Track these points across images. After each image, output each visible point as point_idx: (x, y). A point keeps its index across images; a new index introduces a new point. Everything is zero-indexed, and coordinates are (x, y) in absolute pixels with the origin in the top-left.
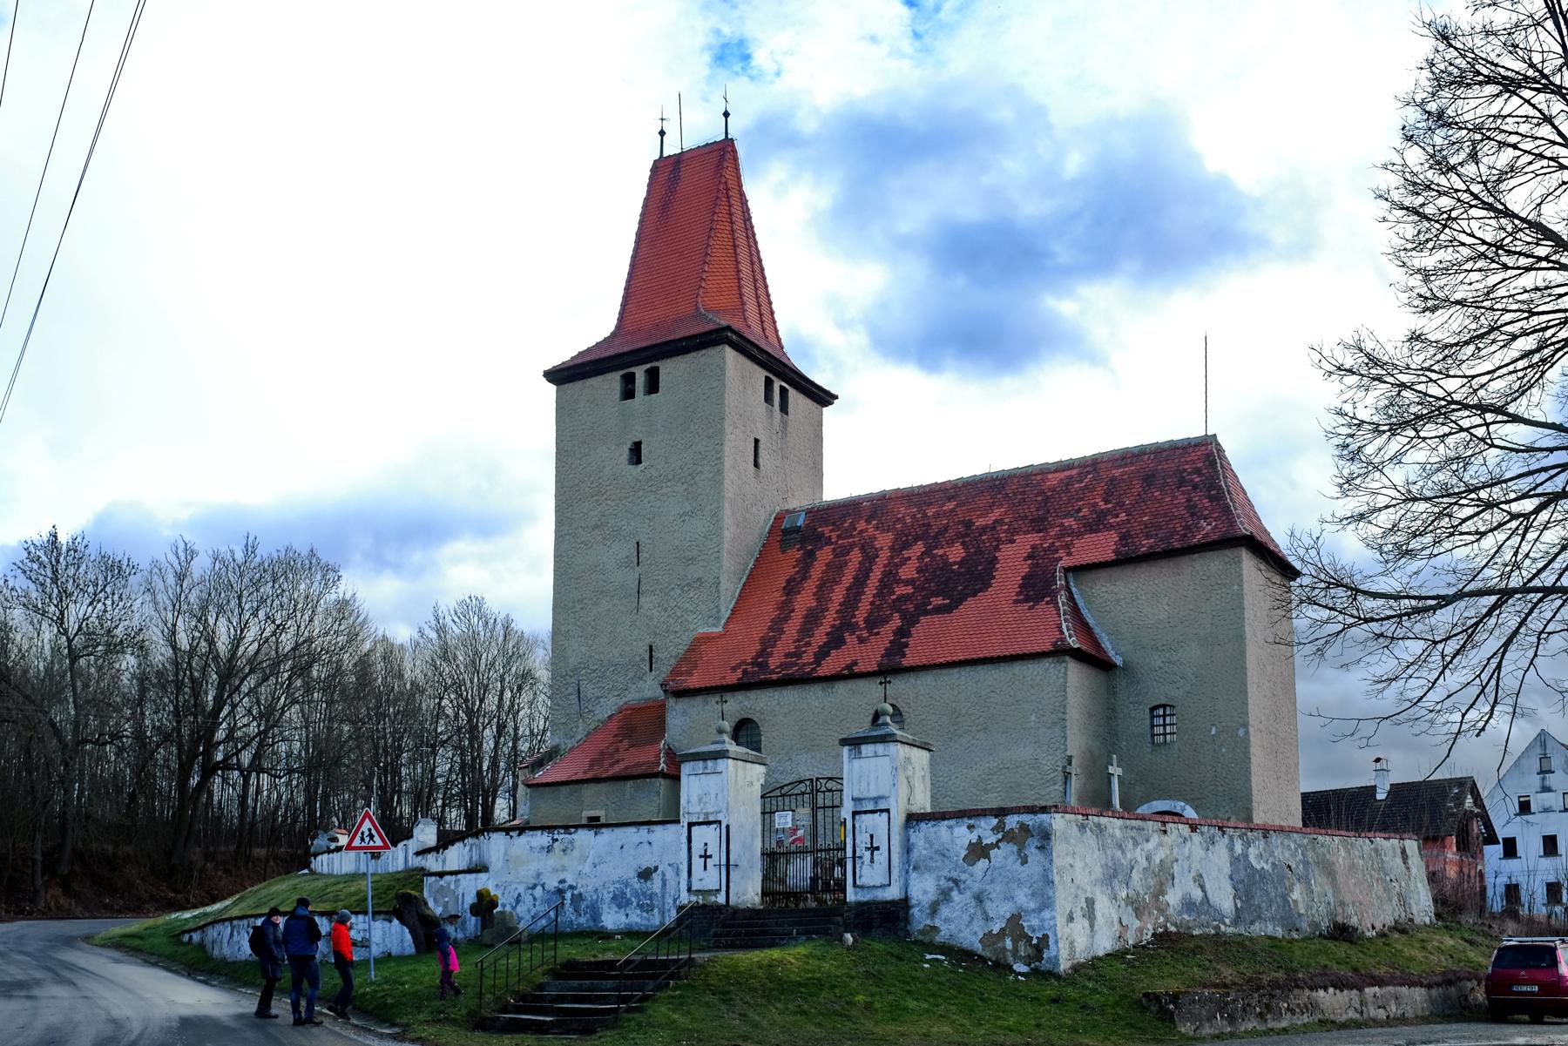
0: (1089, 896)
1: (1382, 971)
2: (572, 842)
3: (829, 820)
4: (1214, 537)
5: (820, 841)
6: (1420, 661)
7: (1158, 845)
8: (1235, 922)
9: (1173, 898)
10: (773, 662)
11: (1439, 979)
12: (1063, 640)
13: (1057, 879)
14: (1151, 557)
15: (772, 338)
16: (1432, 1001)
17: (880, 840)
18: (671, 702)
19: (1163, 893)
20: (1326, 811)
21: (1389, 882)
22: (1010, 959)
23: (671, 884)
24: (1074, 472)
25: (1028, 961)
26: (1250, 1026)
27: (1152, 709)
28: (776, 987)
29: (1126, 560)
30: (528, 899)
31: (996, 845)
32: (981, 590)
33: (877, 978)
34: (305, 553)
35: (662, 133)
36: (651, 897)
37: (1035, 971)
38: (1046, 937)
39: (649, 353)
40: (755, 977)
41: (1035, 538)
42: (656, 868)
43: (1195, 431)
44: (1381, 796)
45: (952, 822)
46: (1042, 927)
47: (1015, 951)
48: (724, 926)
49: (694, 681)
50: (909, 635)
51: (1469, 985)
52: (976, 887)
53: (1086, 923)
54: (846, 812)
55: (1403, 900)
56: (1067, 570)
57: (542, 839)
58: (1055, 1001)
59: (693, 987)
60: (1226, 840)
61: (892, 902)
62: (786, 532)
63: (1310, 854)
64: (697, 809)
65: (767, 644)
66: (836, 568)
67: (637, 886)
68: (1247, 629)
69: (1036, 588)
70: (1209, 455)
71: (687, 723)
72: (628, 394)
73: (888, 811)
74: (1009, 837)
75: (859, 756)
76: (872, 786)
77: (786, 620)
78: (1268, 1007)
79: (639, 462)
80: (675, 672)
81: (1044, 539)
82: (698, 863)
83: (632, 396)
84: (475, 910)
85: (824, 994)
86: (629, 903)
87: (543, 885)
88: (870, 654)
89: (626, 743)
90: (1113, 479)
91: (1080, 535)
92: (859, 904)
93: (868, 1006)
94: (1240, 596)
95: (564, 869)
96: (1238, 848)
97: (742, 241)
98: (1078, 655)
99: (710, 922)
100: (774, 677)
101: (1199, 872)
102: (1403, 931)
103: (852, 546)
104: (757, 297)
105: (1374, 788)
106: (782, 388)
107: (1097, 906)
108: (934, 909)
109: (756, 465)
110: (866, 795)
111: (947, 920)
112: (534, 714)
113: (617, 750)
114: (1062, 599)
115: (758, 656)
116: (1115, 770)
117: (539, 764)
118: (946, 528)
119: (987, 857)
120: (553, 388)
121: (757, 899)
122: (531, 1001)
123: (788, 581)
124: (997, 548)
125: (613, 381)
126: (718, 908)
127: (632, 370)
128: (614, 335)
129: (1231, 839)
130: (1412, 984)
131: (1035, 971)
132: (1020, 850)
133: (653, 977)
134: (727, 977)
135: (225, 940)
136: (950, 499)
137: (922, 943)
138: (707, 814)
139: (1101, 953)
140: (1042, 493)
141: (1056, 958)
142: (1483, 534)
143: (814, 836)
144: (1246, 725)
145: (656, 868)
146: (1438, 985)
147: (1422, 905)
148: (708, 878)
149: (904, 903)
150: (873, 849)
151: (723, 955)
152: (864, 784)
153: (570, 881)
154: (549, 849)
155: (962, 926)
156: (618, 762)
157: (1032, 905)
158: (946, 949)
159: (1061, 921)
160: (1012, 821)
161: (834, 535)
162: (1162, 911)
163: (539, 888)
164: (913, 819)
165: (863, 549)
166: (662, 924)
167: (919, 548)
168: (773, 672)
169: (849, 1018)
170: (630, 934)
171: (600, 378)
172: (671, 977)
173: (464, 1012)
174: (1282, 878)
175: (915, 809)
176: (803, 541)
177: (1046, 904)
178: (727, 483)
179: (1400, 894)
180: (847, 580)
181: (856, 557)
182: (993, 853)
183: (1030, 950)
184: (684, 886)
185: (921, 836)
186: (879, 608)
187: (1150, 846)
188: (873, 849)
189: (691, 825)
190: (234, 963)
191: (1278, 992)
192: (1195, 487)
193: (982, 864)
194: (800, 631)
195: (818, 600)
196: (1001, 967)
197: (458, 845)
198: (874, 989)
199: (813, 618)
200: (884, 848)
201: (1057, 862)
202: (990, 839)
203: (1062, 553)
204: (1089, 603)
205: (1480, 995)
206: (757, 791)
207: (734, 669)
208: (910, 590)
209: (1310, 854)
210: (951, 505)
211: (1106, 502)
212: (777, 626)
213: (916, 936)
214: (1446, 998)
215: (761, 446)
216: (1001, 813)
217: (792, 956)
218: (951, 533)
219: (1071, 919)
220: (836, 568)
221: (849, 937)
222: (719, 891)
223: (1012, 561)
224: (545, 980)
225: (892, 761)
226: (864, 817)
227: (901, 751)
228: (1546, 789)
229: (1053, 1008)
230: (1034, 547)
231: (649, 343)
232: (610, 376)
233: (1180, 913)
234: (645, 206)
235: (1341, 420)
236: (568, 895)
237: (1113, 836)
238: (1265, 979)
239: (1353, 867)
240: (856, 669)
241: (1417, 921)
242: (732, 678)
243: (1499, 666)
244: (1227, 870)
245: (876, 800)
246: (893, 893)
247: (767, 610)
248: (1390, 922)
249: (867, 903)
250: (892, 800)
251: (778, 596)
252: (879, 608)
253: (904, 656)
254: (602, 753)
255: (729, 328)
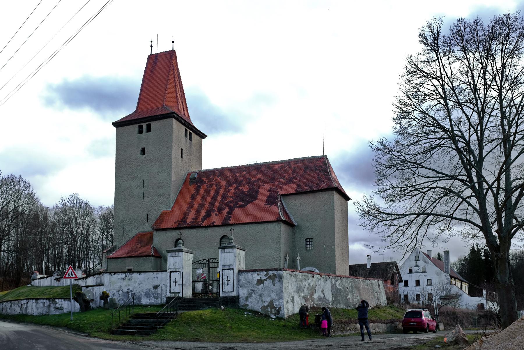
0: (293, 294)
1: (374, 319)
2: (132, 277)
3: (213, 272)
4: (326, 187)
5: (211, 278)
6: (395, 232)
7: (311, 281)
8: (333, 304)
9: (315, 297)
10: (188, 221)
11: (389, 321)
12: (280, 217)
13: (284, 290)
14: (307, 192)
15: (187, 116)
16: (387, 328)
17: (231, 278)
18: (155, 232)
19: (313, 295)
20: (357, 271)
21: (375, 293)
22: (270, 314)
23: (164, 292)
24: (283, 165)
25: (275, 315)
26: (339, 334)
27: (306, 239)
28: (203, 322)
29: (299, 193)
30: (117, 295)
31: (266, 280)
32: (254, 200)
33: (232, 319)
34: (18, 176)
35: (151, 46)
36: (158, 294)
37: (277, 318)
38: (280, 307)
39: (147, 119)
40: (196, 318)
41: (271, 185)
42: (159, 285)
43: (320, 154)
44: (368, 267)
45: (252, 273)
46: (279, 305)
47: (271, 312)
48: (181, 304)
49: (162, 226)
50: (231, 214)
51: (397, 323)
52: (260, 292)
53: (292, 304)
54: (219, 269)
55: (378, 298)
56: (281, 195)
57: (122, 276)
58: (284, 326)
59: (178, 321)
60: (330, 280)
61: (234, 297)
62: (191, 179)
63: (353, 284)
64: (173, 267)
65: (186, 215)
66: (208, 191)
67: (153, 291)
68: (335, 216)
69: (271, 201)
70: (325, 162)
71: (162, 241)
72: (140, 132)
73: (233, 269)
74: (269, 277)
75: (224, 252)
76: (228, 261)
77: (192, 207)
78: (344, 328)
79: (144, 154)
80: (156, 223)
81: (273, 185)
82: (173, 284)
83: (142, 133)
84: (101, 298)
85: (217, 323)
86: (150, 296)
87: (122, 290)
88: (220, 219)
89: (139, 245)
90: (295, 168)
91: (285, 185)
92: (224, 297)
93: (231, 327)
94: (333, 206)
95: (129, 285)
96: (334, 282)
97: (178, 84)
98: (284, 222)
99: (178, 303)
100: (189, 226)
101: (322, 290)
102: (379, 308)
103: (213, 184)
104: (183, 103)
105: (366, 265)
106: (190, 132)
107: (295, 299)
108: (247, 299)
109: (182, 157)
110: (226, 264)
111: (251, 302)
112: (96, 234)
113: (137, 247)
114: (279, 204)
115: (183, 219)
116: (299, 258)
117: (110, 251)
118: (243, 180)
119: (263, 283)
120: (115, 128)
121: (191, 295)
122: (127, 325)
123: (192, 195)
124: (259, 188)
125: (135, 127)
126: (179, 298)
127: (142, 124)
128: (135, 112)
129: (332, 279)
130: (382, 323)
131: (277, 318)
132: (273, 282)
133: (166, 318)
134: (188, 318)
135: (8, 308)
136: (244, 171)
137: (243, 309)
138: (176, 269)
139: (296, 313)
140: (273, 171)
141: (284, 314)
142: (413, 196)
143: (209, 276)
144: (334, 245)
145: (159, 285)
146: (389, 323)
147: (383, 300)
148: (176, 289)
149: (238, 297)
150: (228, 281)
151: (186, 312)
152: (226, 261)
153: (131, 289)
154: (124, 279)
155: (255, 304)
156: (137, 251)
157: (276, 298)
158: (250, 311)
159: (285, 303)
160: (271, 273)
161: (207, 181)
162: (312, 301)
163: (121, 291)
164: (240, 272)
165: (216, 186)
166: (161, 302)
167: (234, 186)
168: (188, 224)
169: (226, 330)
170: (152, 306)
171: (131, 126)
172: (171, 318)
173: (107, 329)
174: (346, 291)
175: (241, 269)
176: (197, 182)
177: (281, 298)
178: (173, 162)
179: (377, 297)
180: (211, 195)
181: (214, 188)
182: (265, 282)
183: (276, 312)
184: (168, 291)
185: (243, 277)
186: (222, 205)
187: (309, 281)
188: (228, 281)
189: (171, 272)
190: (13, 315)
191: (346, 324)
192: (320, 171)
193: (261, 285)
194: (196, 211)
195: (202, 201)
196: (267, 316)
197: (91, 277)
198: (231, 322)
199: (200, 207)
200: (232, 280)
201: (284, 285)
202: (264, 278)
203: (279, 190)
204: (287, 206)
205: (400, 326)
206: (191, 262)
207: (175, 223)
208: (231, 199)
209: (353, 284)
210: (244, 173)
211: (293, 175)
212: (189, 209)
213: (241, 307)
214: (391, 327)
215: (184, 151)
216: (267, 270)
217: (206, 312)
218: (244, 182)
219: (288, 302)
220: (208, 191)
221: (222, 307)
222: (179, 293)
223: (264, 192)
224: (130, 319)
225: (235, 254)
226: (225, 271)
227: (237, 251)
228: (417, 266)
229: (284, 328)
230: (270, 188)
231: (146, 116)
232: (134, 126)
233: (317, 301)
234: (146, 70)
235: (376, 163)
236: (130, 293)
237: (299, 278)
238: (343, 321)
239: (365, 288)
240: (215, 224)
241: (382, 305)
242: (175, 226)
243: (417, 234)
244: (330, 289)
245: (229, 266)
246: (234, 294)
247: (185, 204)
248: (375, 305)
249: (225, 297)
250: (234, 266)
251: (189, 200)
252: (222, 205)
253: (230, 220)
254: (132, 248)
255: (174, 113)
